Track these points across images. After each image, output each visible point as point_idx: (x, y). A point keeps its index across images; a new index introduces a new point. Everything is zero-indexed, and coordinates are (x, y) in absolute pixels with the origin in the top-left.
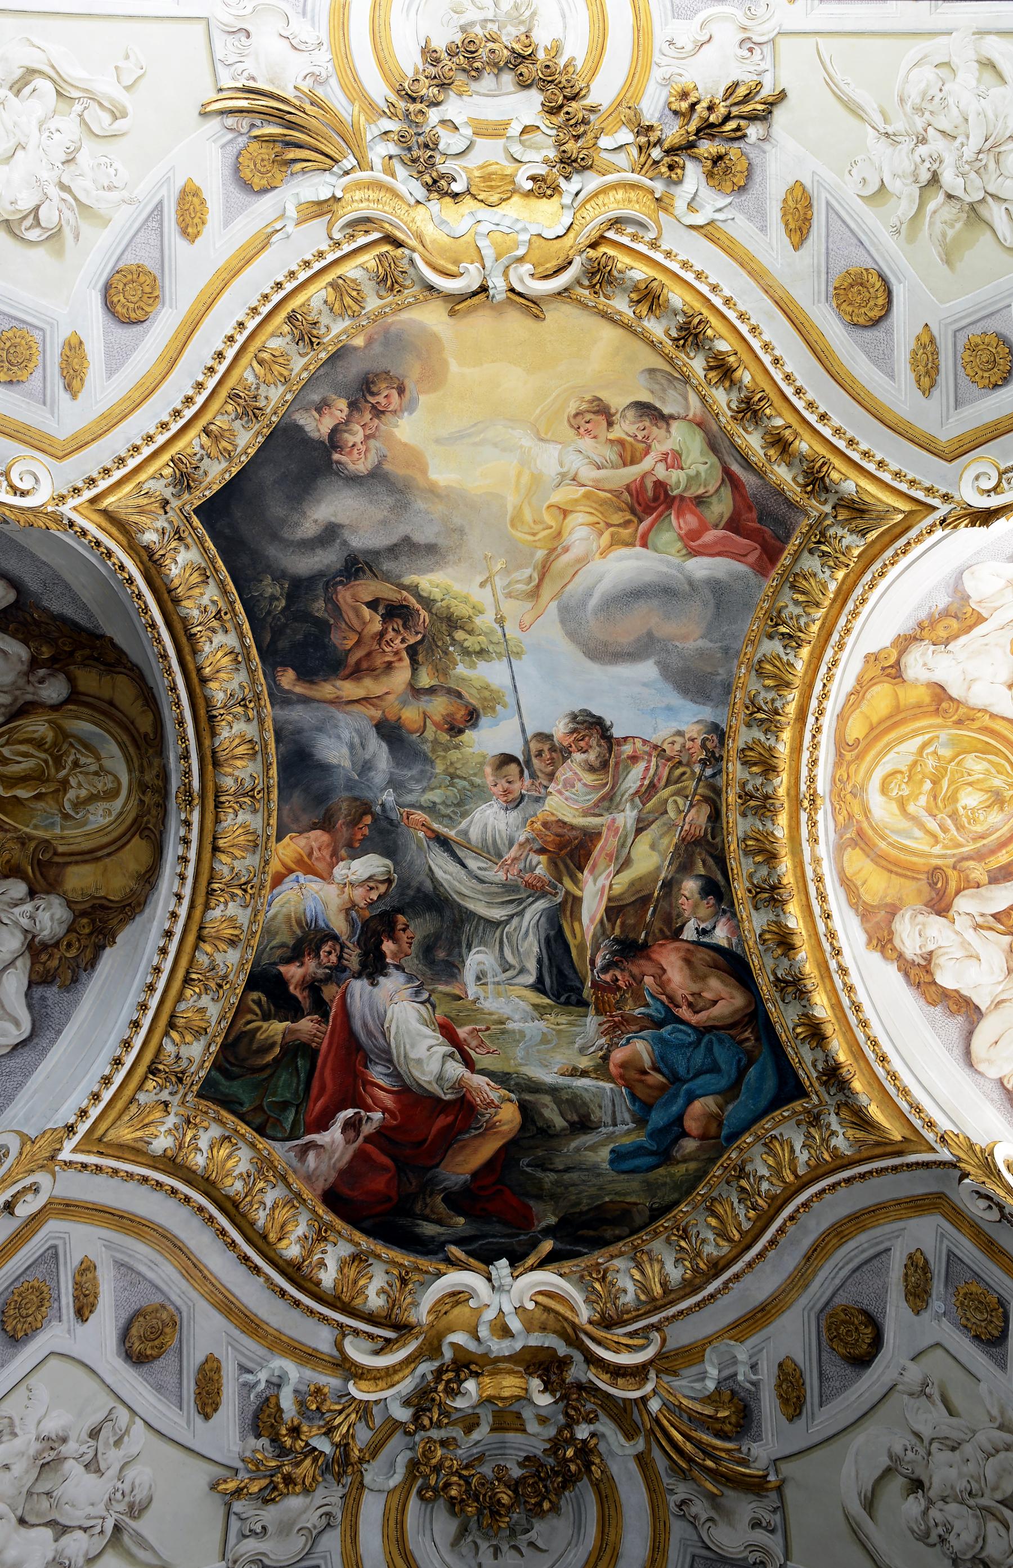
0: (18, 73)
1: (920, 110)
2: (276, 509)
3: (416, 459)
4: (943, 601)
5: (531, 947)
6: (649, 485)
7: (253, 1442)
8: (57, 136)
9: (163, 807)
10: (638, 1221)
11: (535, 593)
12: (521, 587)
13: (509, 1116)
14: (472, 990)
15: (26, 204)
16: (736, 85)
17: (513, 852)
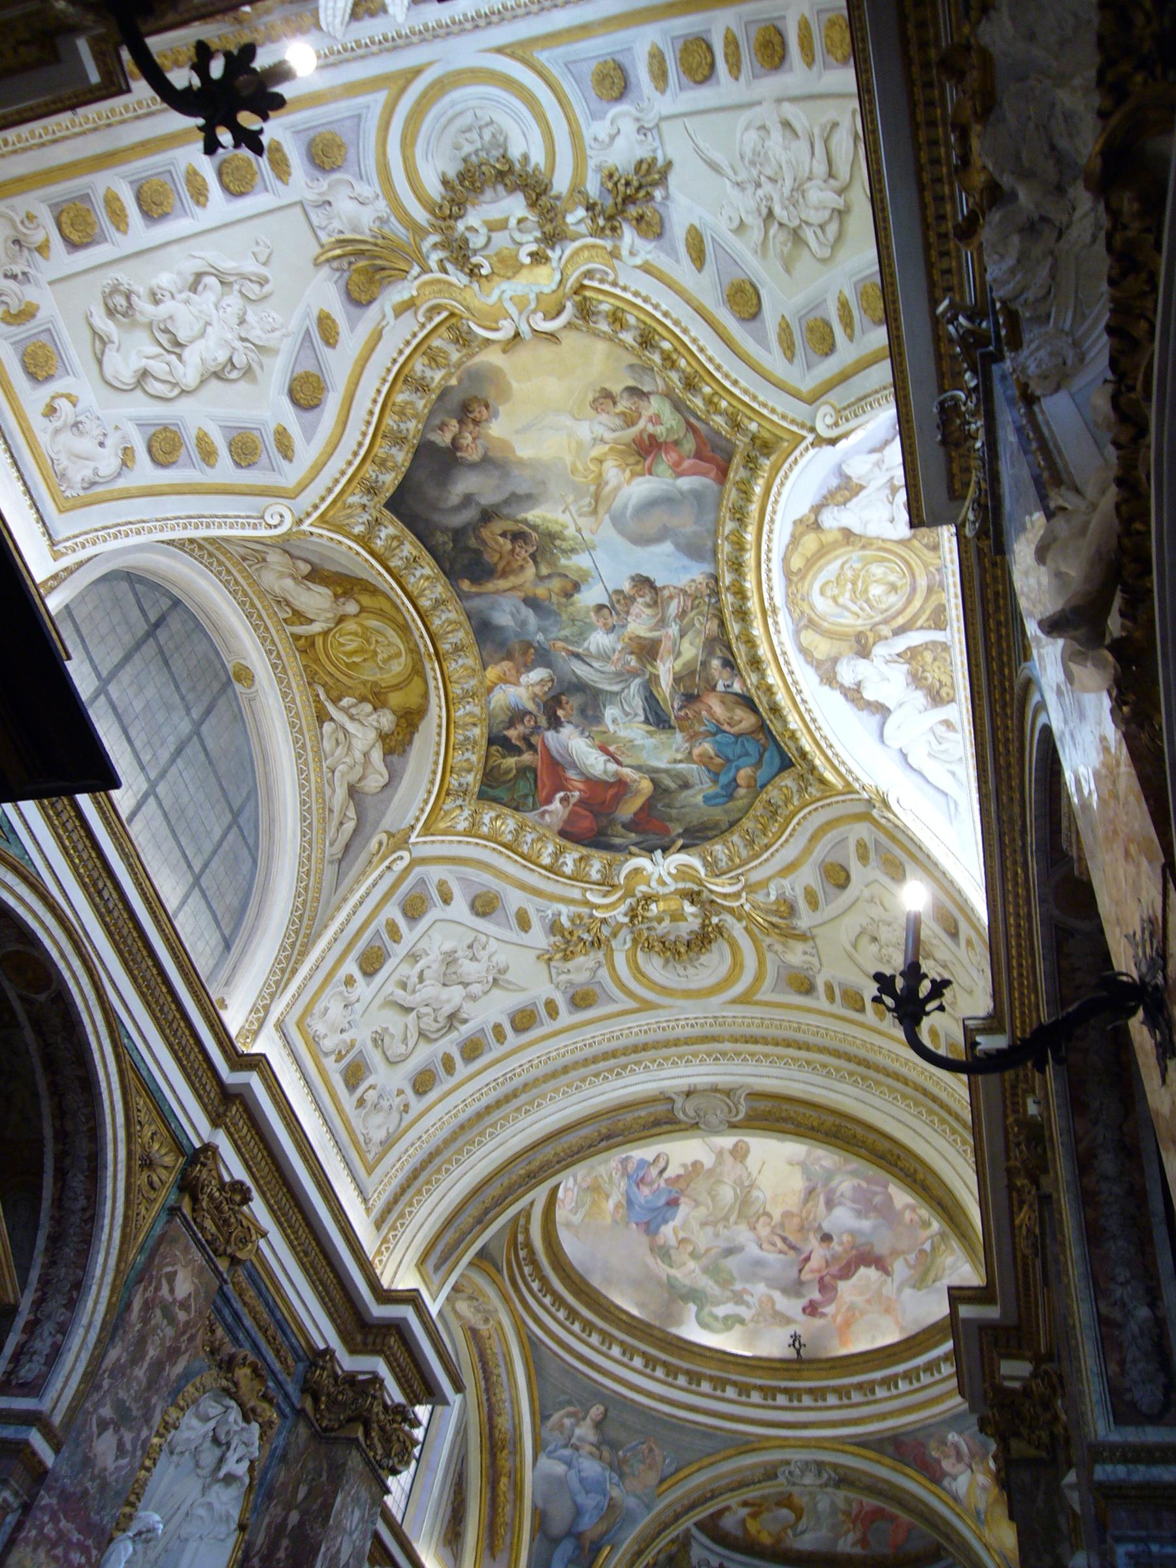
0: (191, 279)
1: (753, 163)
2: (432, 492)
3: (507, 446)
4: (834, 482)
5: (638, 703)
6: (645, 437)
7: (552, 939)
8: (229, 310)
9: (421, 660)
10: (724, 828)
11: (594, 512)
12: (586, 509)
13: (646, 786)
14: (612, 728)
15: (222, 357)
16: (641, 162)
17: (616, 655)
